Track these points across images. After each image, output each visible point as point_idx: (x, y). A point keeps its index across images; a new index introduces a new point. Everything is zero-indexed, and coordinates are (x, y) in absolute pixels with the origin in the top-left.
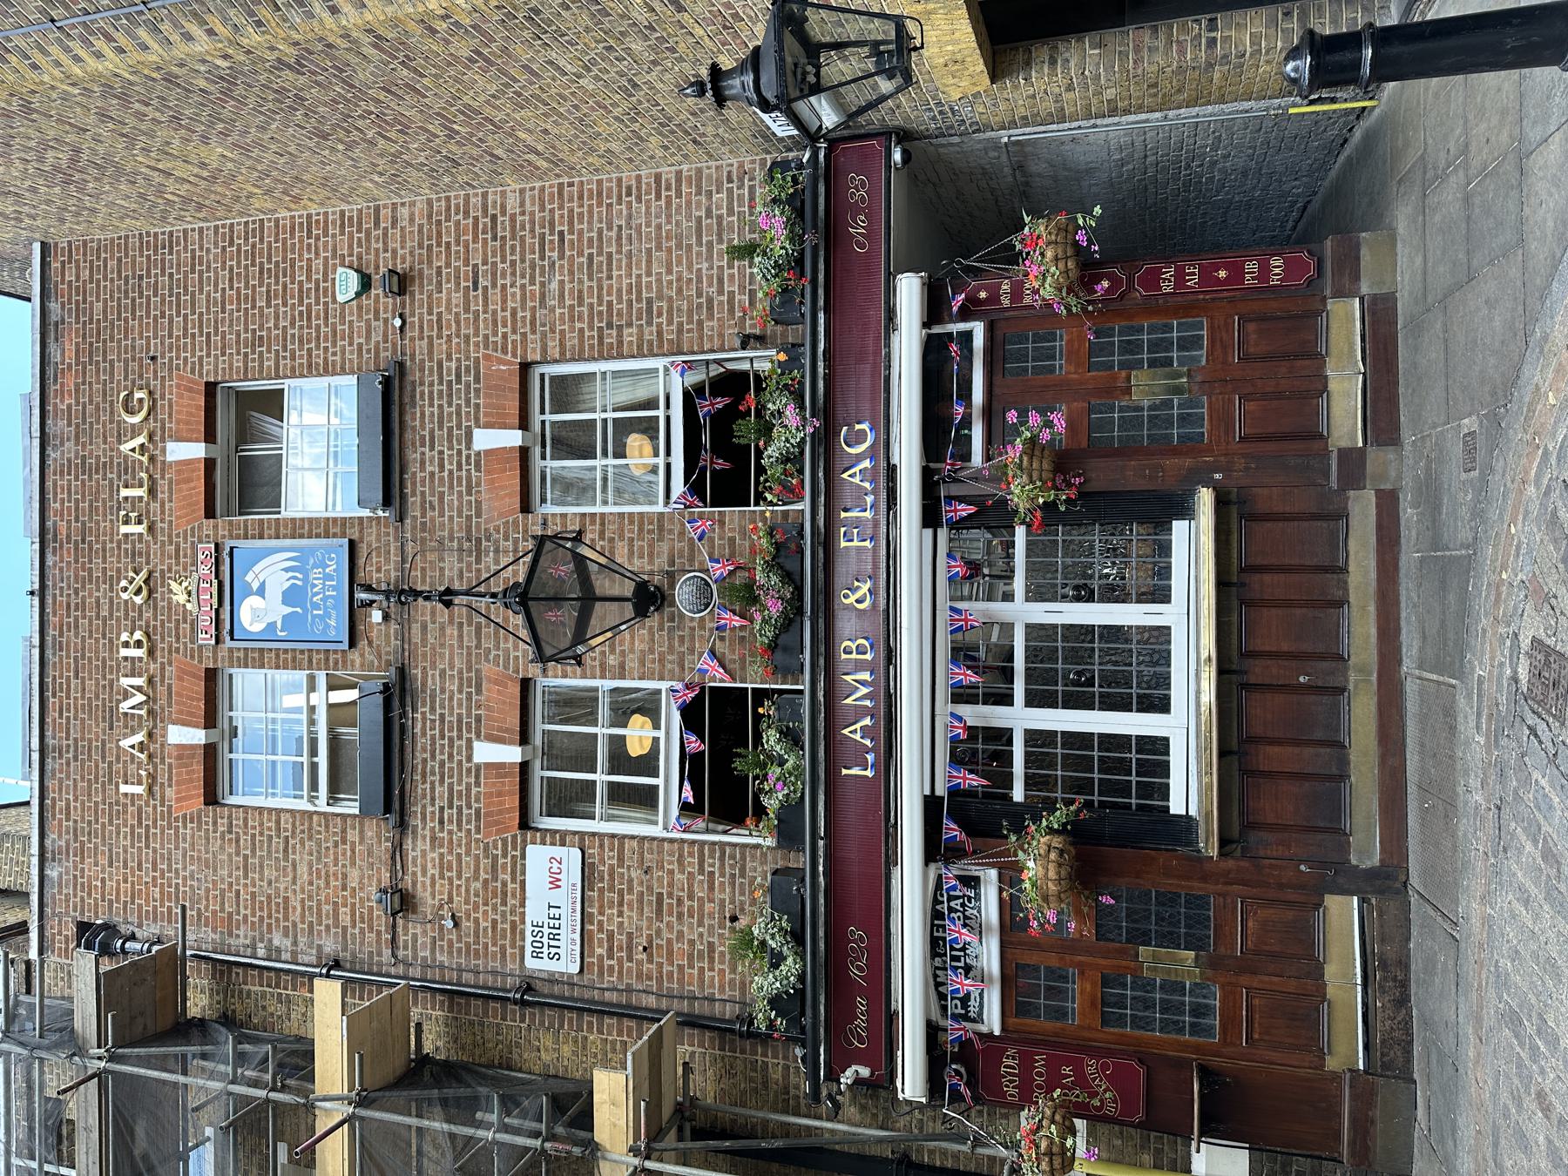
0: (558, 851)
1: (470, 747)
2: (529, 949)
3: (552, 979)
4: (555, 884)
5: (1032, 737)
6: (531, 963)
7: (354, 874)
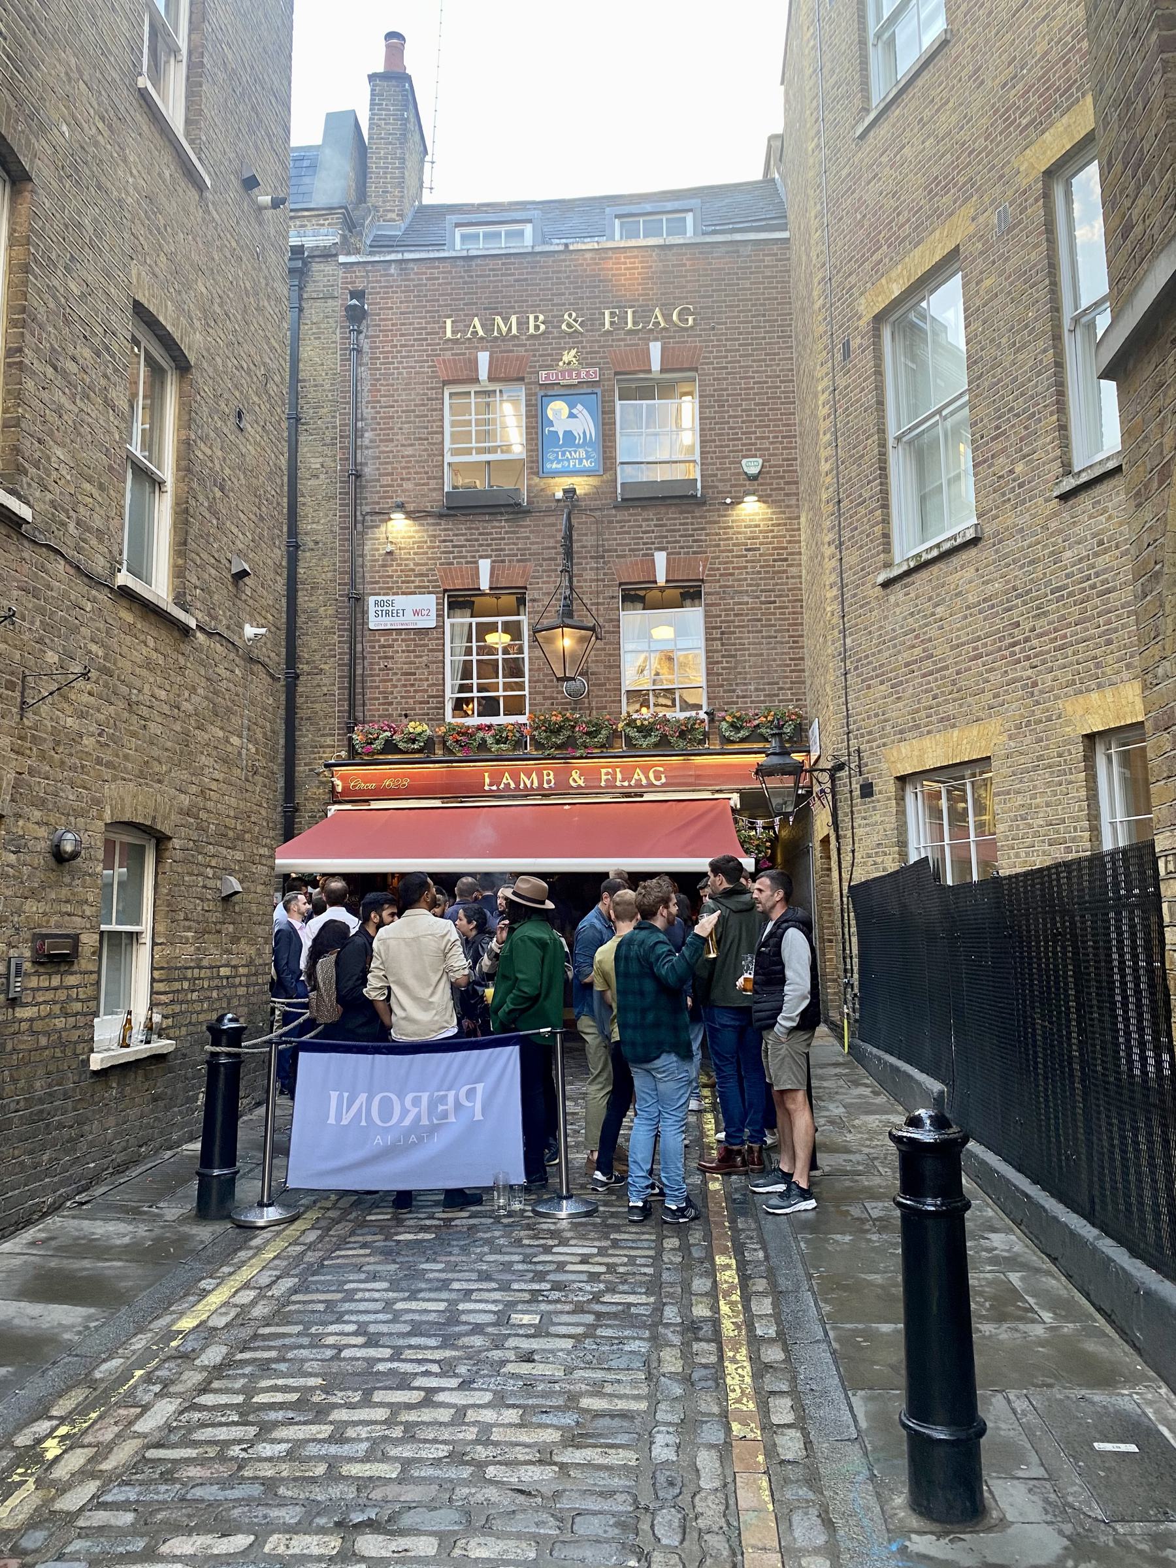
0: (433, 613)
1: (486, 557)
2: (379, 598)
3: (364, 613)
4: (416, 613)
5: (453, 443)
6: (372, 600)
7: (408, 485)
